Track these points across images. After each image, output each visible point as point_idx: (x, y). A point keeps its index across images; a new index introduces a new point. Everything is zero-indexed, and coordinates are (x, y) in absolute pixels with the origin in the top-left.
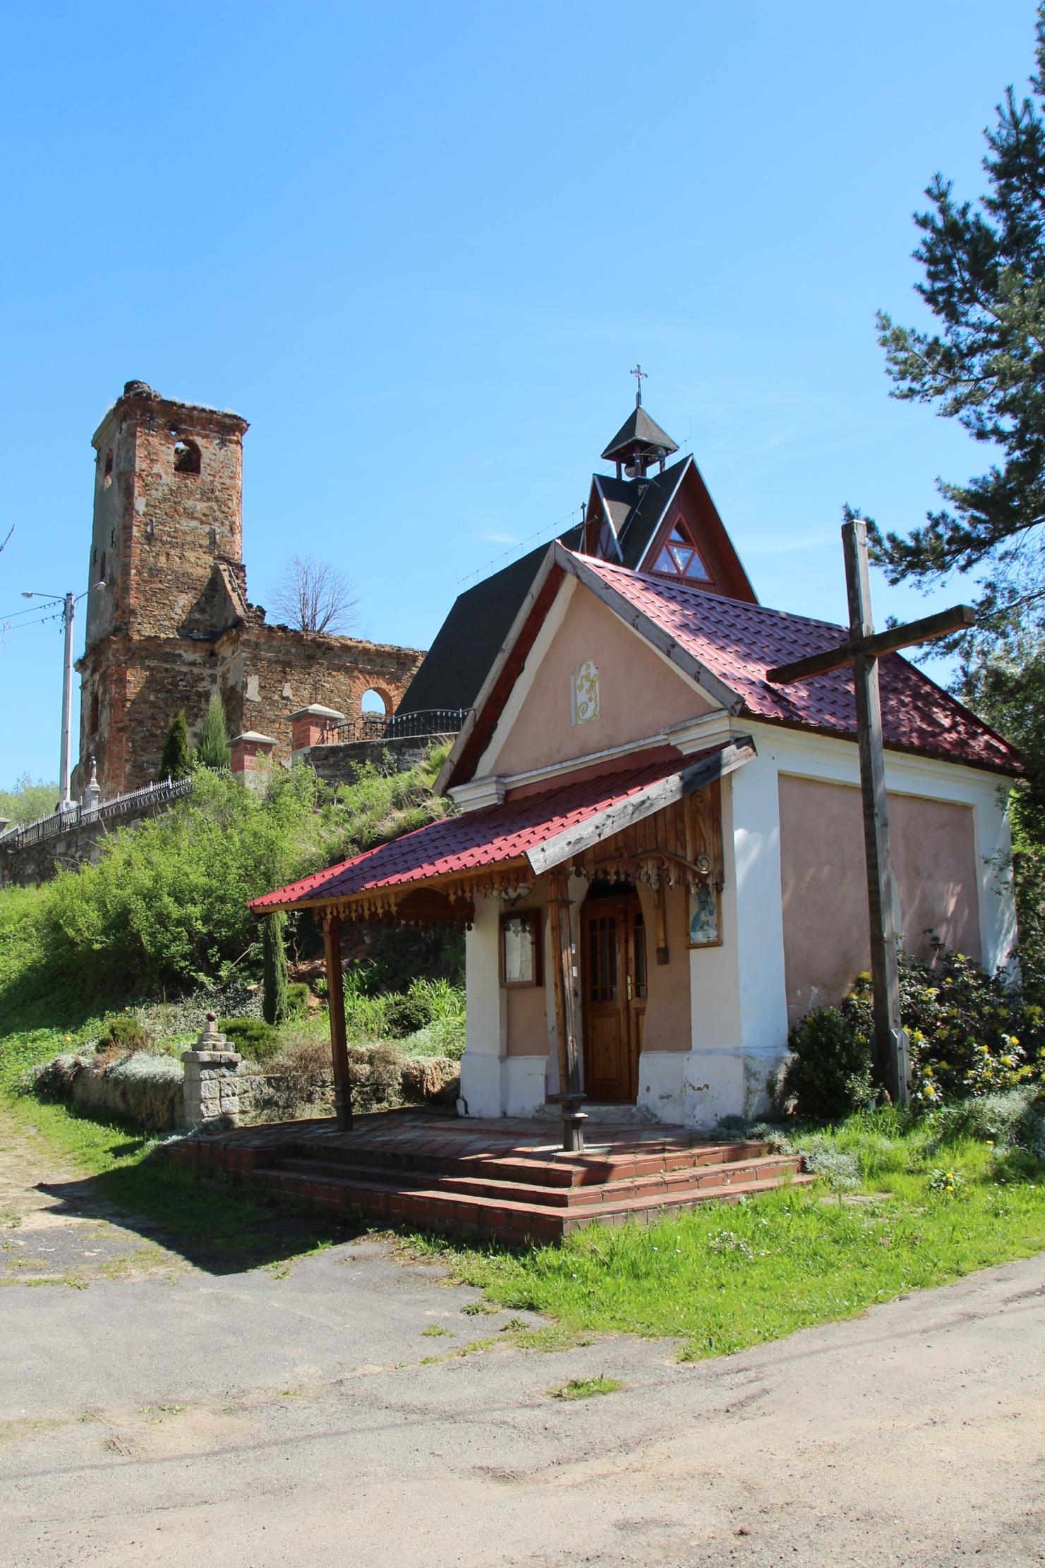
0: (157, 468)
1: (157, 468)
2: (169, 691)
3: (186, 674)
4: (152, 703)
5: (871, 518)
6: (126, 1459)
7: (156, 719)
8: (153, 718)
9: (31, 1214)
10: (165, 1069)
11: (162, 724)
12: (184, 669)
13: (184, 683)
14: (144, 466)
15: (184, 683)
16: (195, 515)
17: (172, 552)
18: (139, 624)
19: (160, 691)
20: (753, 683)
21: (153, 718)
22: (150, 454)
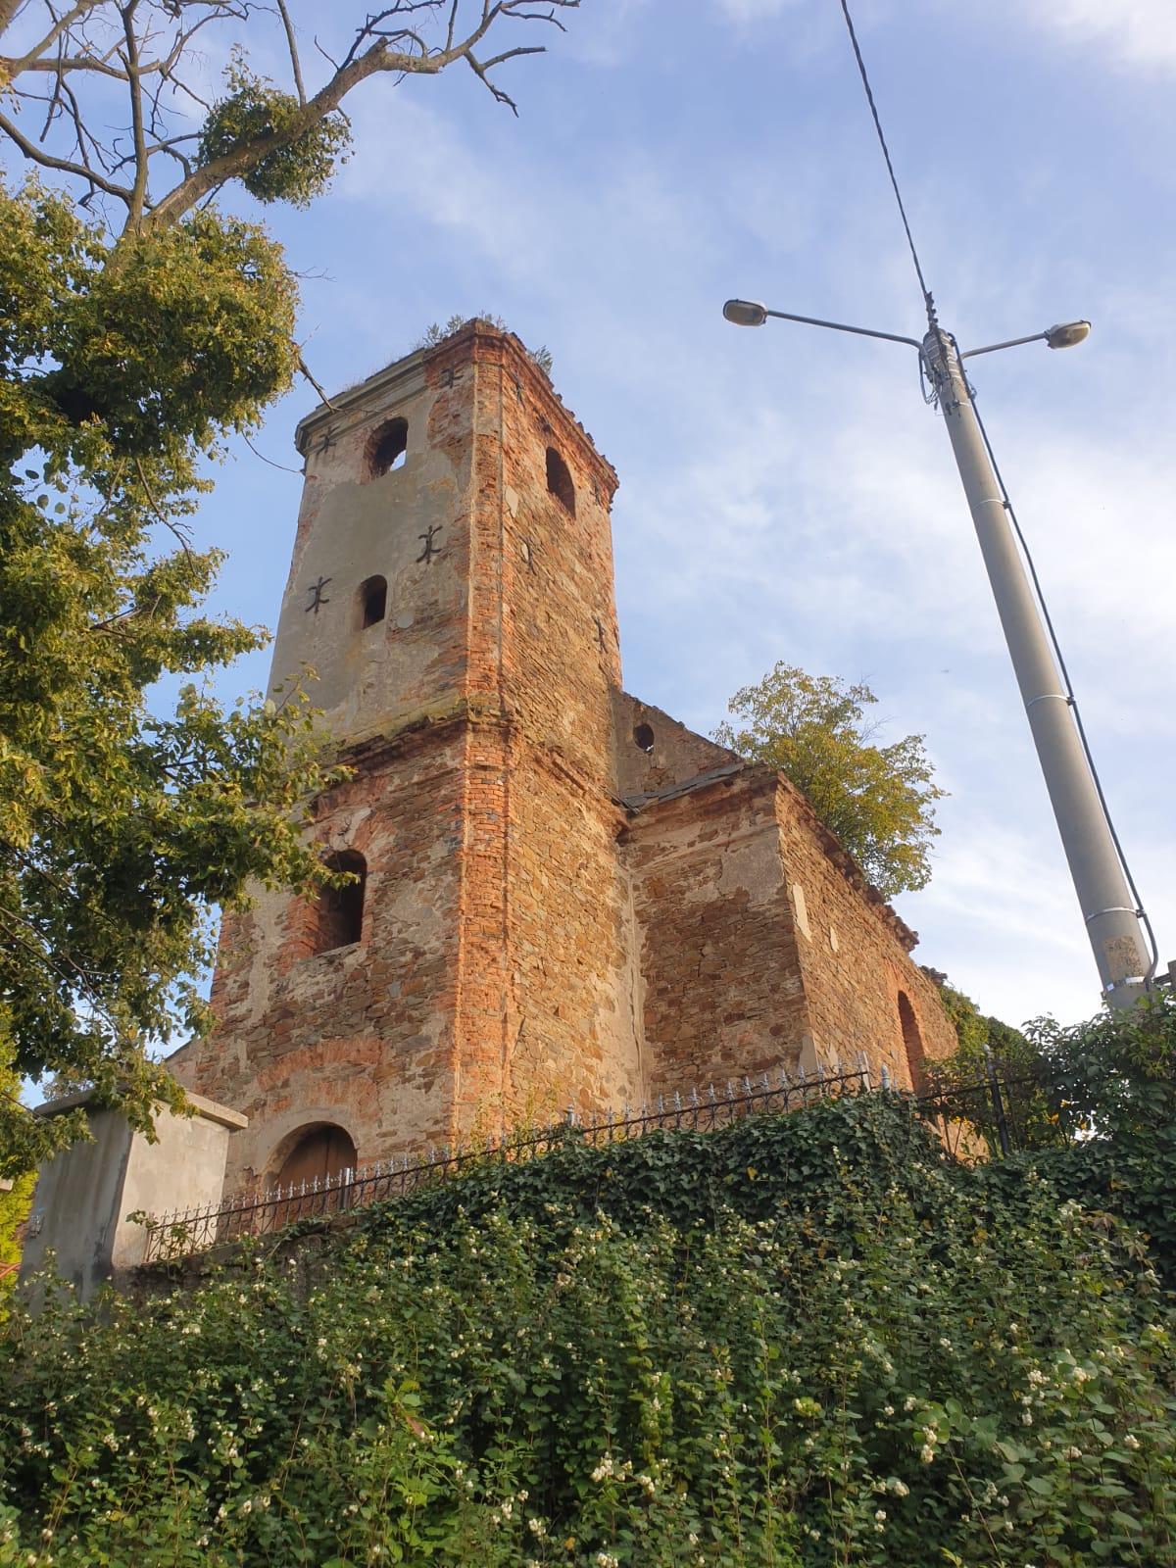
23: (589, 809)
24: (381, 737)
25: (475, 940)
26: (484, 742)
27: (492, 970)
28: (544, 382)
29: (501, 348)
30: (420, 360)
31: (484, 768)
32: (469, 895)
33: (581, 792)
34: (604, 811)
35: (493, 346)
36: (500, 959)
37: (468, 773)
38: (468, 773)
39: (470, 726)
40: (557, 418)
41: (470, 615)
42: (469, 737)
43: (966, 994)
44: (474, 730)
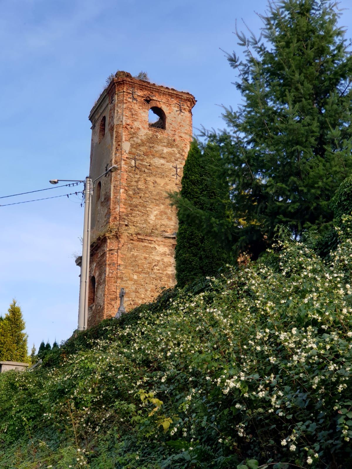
0: (136, 124)
1: (136, 124)
2: (148, 273)
3: (159, 261)
4: (136, 281)
5: (26, 317)
6: (158, 275)
7: (138, 292)
8: (136, 292)
9: (166, 225)
10: (160, 160)
11: (143, 296)
12: (158, 258)
13: (158, 268)
14: (129, 122)
15: (158, 268)
16: (164, 156)
17: (148, 179)
18: (126, 225)
19: (140, 273)
20: (162, 254)
21: (136, 292)
22: (132, 115)
23: (159, 245)
24: (94, 242)
25: (109, 302)
26: (112, 241)
27: (113, 309)
28: (146, 84)
29: (124, 83)
30: (106, 94)
31: (111, 250)
32: (107, 289)
33: (153, 242)
34: (166, 244)
35: (121, 84)
36: (115, 306)
37: (108, 252)
38: (108, 252)
39: (107, 238)
40: (156, 91)
41: (112, 197)
42: (108, 241)
43: (23, 313)
44: (109, 239)
